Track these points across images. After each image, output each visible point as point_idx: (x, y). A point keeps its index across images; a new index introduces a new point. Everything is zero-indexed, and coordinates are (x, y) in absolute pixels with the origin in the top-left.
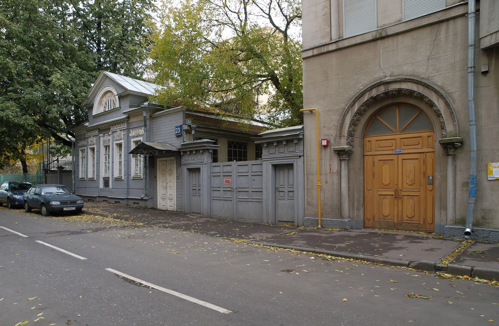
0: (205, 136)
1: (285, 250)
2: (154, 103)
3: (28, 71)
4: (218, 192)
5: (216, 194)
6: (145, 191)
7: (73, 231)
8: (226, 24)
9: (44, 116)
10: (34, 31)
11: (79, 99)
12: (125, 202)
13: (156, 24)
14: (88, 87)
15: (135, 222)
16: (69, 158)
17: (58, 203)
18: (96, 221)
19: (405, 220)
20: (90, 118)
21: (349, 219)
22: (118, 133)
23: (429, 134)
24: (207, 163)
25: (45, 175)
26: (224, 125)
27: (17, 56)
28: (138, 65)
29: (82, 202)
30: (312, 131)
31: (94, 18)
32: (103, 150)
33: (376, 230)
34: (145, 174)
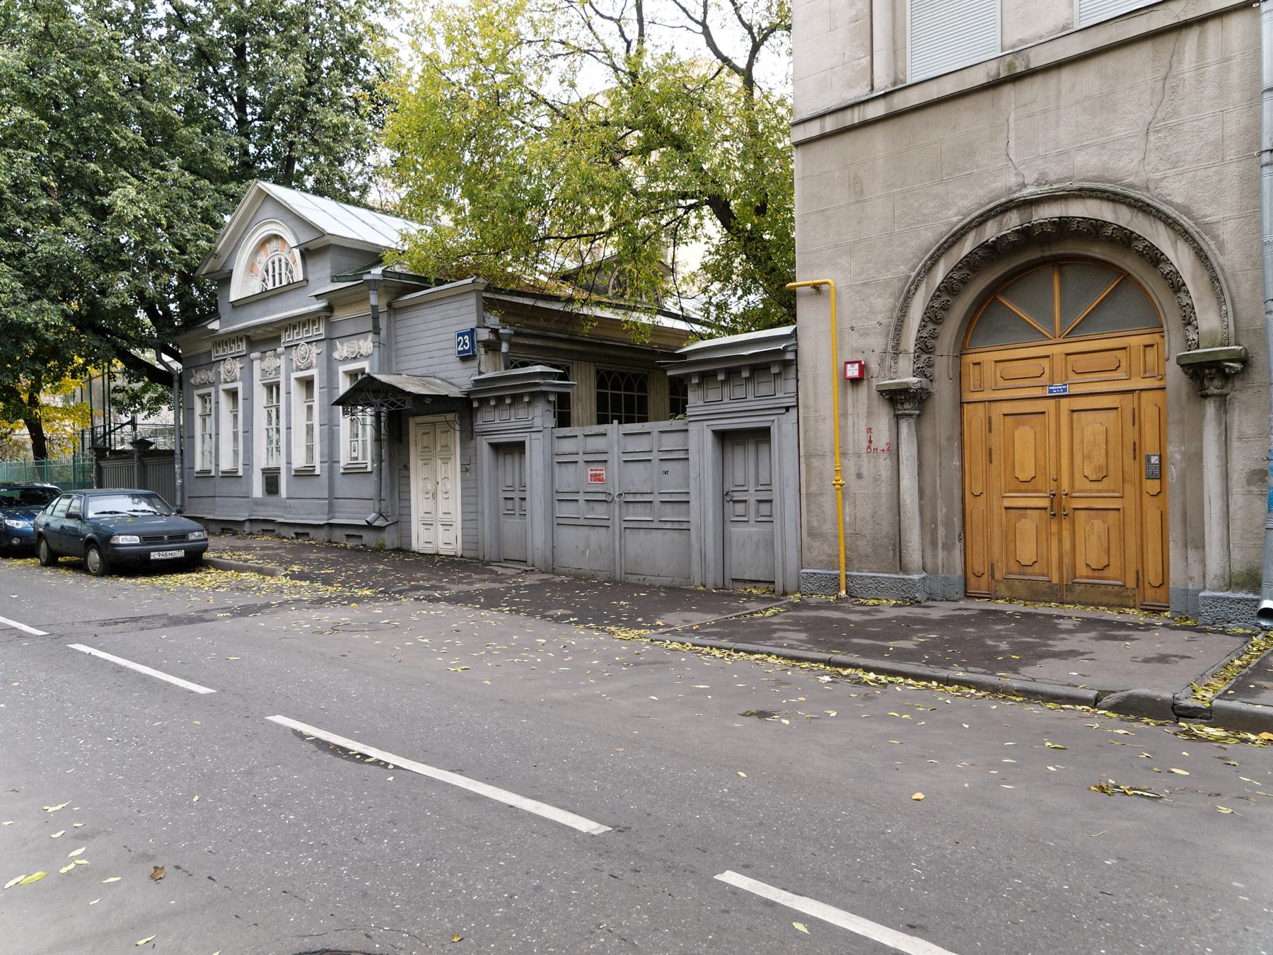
1: (752, 657)
2: (397, 269)
3: (45, 179)
4: (574, 504)
5: (566, 510)
7: (178, 617)
8: (587, 52)
9: (92, 303)
10: (58, 67)
11: (192, 255)
12: (322, 535)
13: (397, 50)
14: (217, 226)
15: (351, 587)
16: (166, 416)
17: (136, 540)
18: (242, 588)
19: (1081, 577)
20: (224, 309)
21: (924, 575)
22: (303, 349)
23: (1147, 339)
25: (98, 465)
26: (587, 328)
27: (12, 136)
28: (351, 166)
30: (820, 340)
31: (225, 33)
32: (260, 395)
33: (1000, 605)
34: (378, 458)
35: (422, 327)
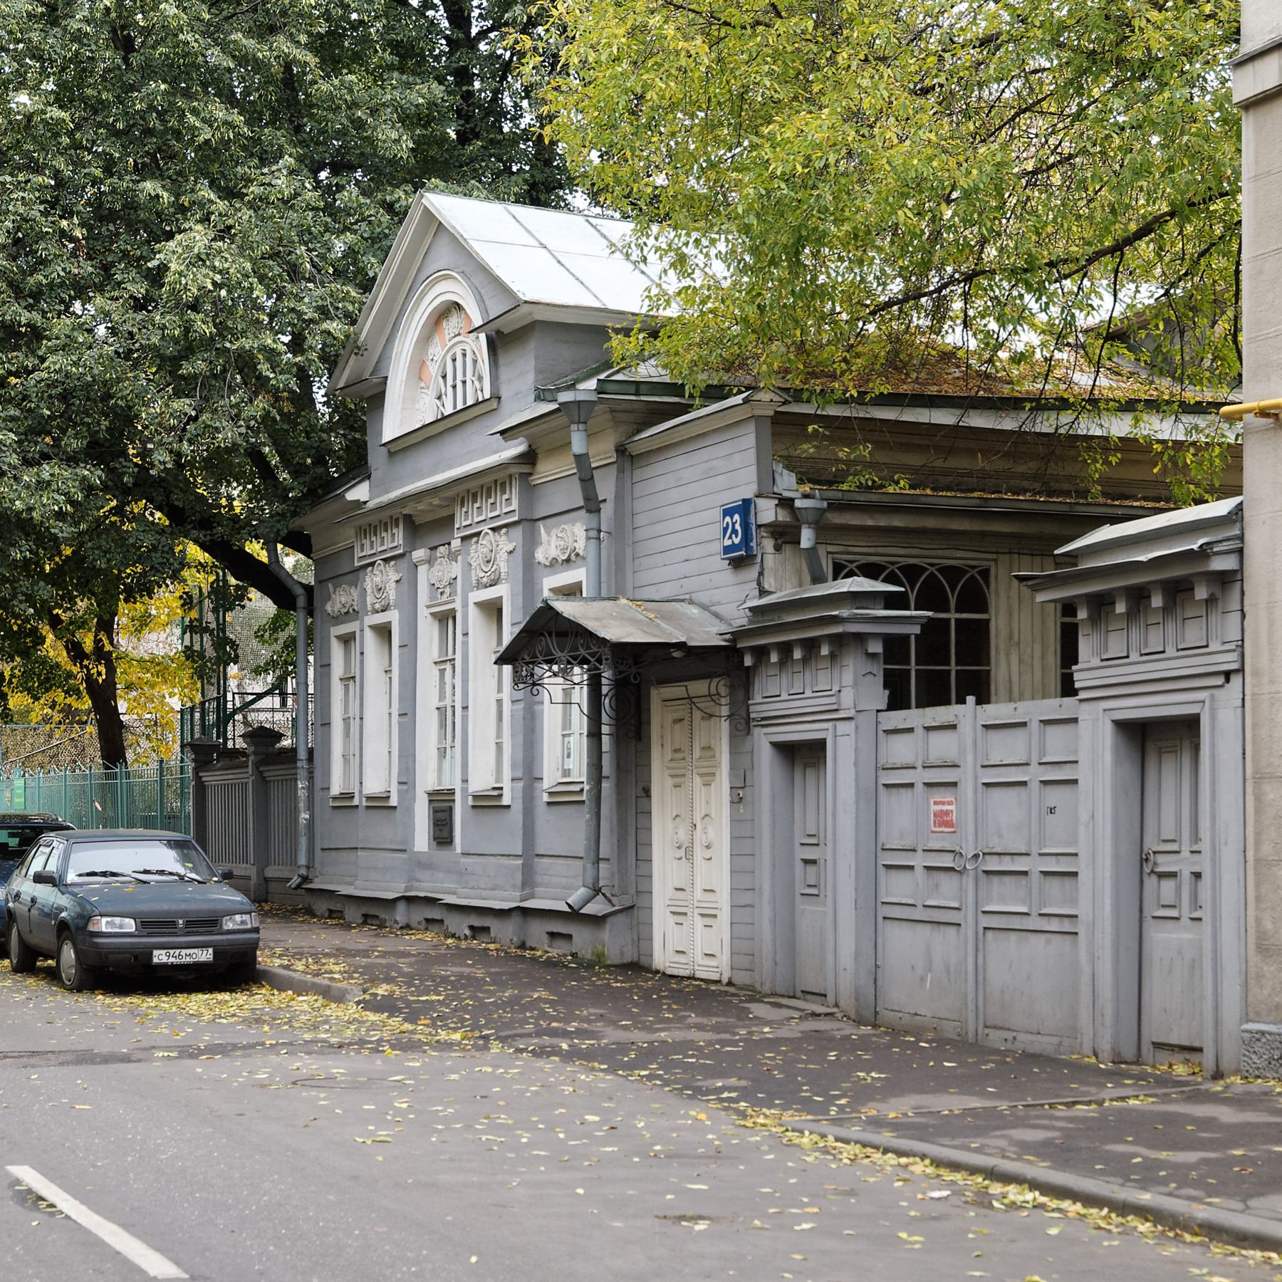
0: (902, 551)
3: (64, 223)
5: (898, 888)
6: (589, 866)
12: (505, 932)
17: (130, 925)
20: (376, 458)
24: (852, 713)
25: (198, 779)
29: (250, 921)
32: (428, 631)
35: (674, 495)
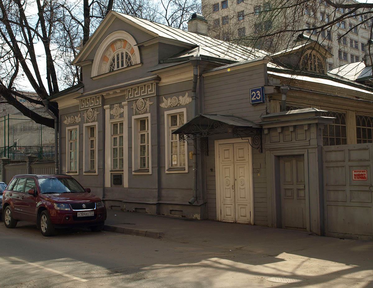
25: (4, 168)
